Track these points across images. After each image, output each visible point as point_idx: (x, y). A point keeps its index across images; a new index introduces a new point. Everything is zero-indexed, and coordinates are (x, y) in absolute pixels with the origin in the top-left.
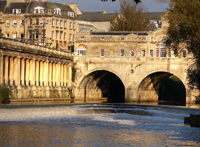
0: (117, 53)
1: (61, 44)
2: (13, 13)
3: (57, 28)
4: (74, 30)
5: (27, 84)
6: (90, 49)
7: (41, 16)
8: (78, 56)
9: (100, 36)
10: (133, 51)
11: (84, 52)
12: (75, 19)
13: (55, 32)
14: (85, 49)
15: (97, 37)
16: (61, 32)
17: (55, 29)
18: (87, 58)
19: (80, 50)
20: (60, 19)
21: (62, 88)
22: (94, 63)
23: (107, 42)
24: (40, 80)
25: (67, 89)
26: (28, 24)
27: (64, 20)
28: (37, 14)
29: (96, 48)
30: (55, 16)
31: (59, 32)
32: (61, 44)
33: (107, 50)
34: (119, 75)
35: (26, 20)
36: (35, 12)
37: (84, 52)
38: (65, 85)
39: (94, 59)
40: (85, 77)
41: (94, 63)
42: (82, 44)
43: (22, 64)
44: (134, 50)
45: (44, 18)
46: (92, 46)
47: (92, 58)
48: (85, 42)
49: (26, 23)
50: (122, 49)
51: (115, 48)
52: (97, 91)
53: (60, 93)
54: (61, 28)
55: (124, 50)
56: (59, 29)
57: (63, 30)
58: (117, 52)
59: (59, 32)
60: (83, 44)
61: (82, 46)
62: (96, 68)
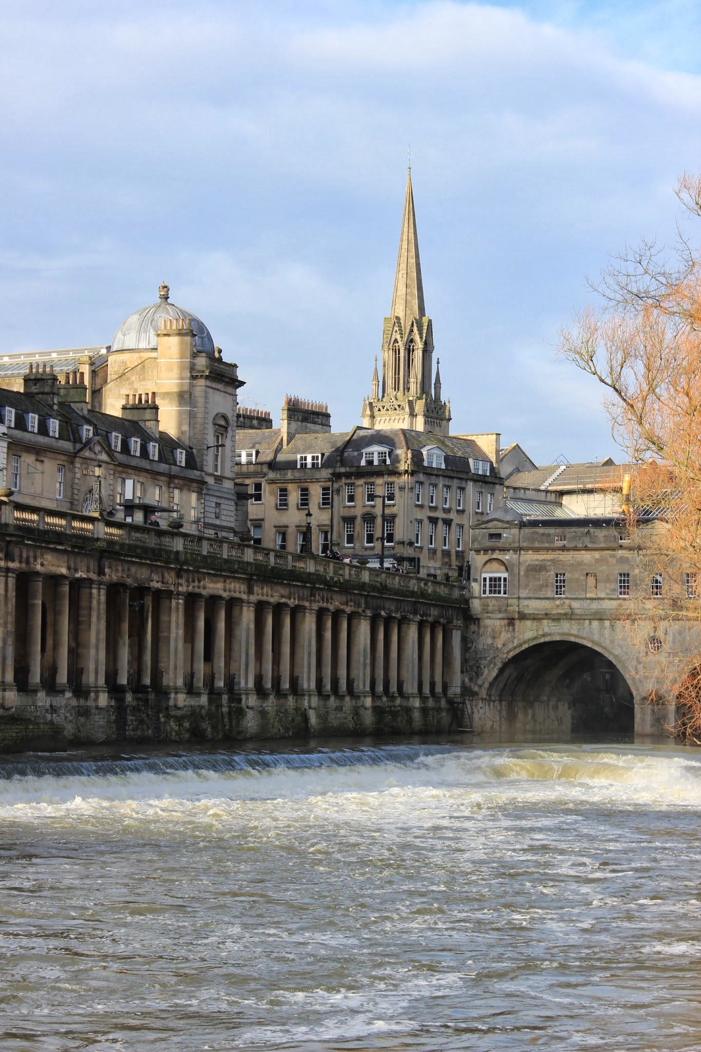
0: (608, 585)
1: (446, 560)
2: (299, 467)
3: (434, 509)
4: (458, 511)
5: (394, 688)
6: (522, 573)
7: (379, 474)
8: (483, 596)
9: (551, 531)
10: (659, 578)
11: (502, 582)
12: (493, 480)
13: (426, 521)
14: (506, 575)
15: (543, 534)
16: (448, 523)
17: (423, 515)
18: (510, 601)
19: (488, 576)
20: (441, 482)
21: (423, 699)
22: (535, 618)
23: (576, 549)
24: (195, 670)
25: (443, 703)
26: (341, 504)
27: (455, 483)
28: (369, 469)
29: (536, 569)
30: (424, 473)
31: (440, 523)
32: (446, 560)
33: (577, 575)
34: (616, 657)
35: (336, 486)
36: (363, 463)
37: (502, 582)
38: (439, 689)
39: (533, 606)
40: (506, 665)
41: (535, 618)
42: (494, 556)
43: (403, 634)
44: (661, 575)
45: (349, 481)
46: (527, 564)
47: (526, 602)
48: (504, 550)
49: (335, 497)
50: (623, 572)
51: (602, 568)
52: (556, 708)
53: (417, 715)
54: (447, 511)
55: (628, 575)
56: (440, 514)
57: (452, 515)
58: (608, 580)
59: (440, 523)
60: (500, 557)
61: (495, 565)
62: (541, 633)
